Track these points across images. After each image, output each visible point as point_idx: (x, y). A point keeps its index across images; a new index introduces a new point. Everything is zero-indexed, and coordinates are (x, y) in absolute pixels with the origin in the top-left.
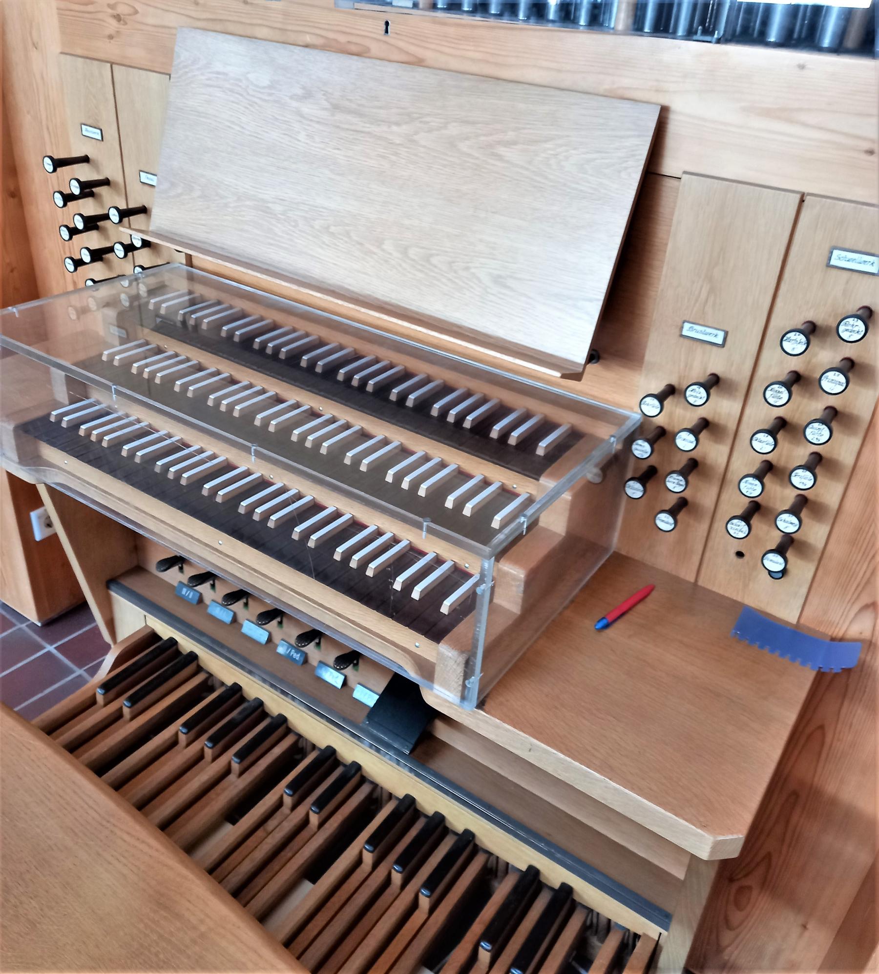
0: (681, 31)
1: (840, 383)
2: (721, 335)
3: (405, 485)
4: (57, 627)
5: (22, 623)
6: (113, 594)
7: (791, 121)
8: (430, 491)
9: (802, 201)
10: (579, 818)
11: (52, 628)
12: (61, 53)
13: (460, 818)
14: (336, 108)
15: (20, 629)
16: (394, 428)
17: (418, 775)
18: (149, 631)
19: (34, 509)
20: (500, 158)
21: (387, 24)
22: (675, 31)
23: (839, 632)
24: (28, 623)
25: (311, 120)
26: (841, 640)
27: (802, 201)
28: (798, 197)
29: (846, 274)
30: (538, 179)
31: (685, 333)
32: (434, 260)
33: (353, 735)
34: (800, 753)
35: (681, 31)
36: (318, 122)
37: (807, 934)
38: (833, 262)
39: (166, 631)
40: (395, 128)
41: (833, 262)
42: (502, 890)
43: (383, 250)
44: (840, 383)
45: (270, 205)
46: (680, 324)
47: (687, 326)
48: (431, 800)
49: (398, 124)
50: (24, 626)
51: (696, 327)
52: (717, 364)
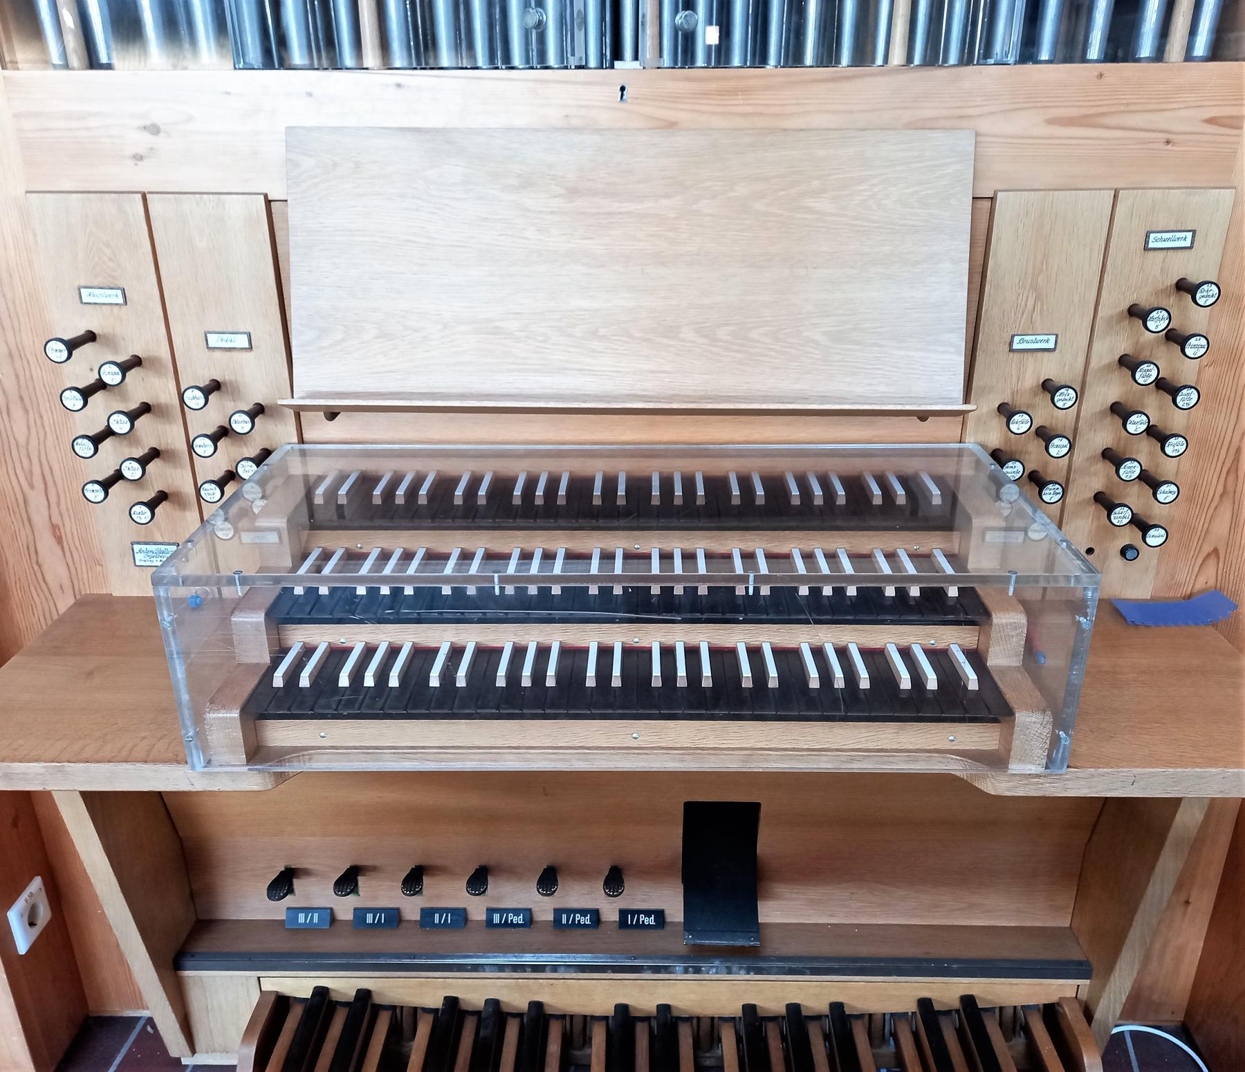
0: (953, 57)
1: (1202, 347)
2: (1053, 338)
7: (1094, 126)
8: (404, 678)
9: (1116, 197)
10: (935, 923)
12: (27, 192)
13: (814, 993)
14: (573, 192)
17: (759, 971)
18: (273, 998)
20: (810, 210)
21: (623, 89)
22: (945, 60)
23: (1187, 590)
25: (541, 212)
26: (1190, 596)
27: (1116, 197)
28: (1112, 193)
29: (1163, 253)
30: (858, 223)
31: (1015, 346)
32: (753, 335)
33: (656, 970)
34: (501, 968)
35: (953, 57)
36: (552, 213)
37: (1190, 908)
38: (1151, 245)
39: (299, 985)
40: (665, 202)
41: (1151, 245)
43: (683, 340)
44: (1202, 347)
45: (498, 324)
46: (1008, 340)
47: (1017, 339)
48: (773, 993)
49: (667, 196)
51: (1026, 338)
52: (1050, 369)
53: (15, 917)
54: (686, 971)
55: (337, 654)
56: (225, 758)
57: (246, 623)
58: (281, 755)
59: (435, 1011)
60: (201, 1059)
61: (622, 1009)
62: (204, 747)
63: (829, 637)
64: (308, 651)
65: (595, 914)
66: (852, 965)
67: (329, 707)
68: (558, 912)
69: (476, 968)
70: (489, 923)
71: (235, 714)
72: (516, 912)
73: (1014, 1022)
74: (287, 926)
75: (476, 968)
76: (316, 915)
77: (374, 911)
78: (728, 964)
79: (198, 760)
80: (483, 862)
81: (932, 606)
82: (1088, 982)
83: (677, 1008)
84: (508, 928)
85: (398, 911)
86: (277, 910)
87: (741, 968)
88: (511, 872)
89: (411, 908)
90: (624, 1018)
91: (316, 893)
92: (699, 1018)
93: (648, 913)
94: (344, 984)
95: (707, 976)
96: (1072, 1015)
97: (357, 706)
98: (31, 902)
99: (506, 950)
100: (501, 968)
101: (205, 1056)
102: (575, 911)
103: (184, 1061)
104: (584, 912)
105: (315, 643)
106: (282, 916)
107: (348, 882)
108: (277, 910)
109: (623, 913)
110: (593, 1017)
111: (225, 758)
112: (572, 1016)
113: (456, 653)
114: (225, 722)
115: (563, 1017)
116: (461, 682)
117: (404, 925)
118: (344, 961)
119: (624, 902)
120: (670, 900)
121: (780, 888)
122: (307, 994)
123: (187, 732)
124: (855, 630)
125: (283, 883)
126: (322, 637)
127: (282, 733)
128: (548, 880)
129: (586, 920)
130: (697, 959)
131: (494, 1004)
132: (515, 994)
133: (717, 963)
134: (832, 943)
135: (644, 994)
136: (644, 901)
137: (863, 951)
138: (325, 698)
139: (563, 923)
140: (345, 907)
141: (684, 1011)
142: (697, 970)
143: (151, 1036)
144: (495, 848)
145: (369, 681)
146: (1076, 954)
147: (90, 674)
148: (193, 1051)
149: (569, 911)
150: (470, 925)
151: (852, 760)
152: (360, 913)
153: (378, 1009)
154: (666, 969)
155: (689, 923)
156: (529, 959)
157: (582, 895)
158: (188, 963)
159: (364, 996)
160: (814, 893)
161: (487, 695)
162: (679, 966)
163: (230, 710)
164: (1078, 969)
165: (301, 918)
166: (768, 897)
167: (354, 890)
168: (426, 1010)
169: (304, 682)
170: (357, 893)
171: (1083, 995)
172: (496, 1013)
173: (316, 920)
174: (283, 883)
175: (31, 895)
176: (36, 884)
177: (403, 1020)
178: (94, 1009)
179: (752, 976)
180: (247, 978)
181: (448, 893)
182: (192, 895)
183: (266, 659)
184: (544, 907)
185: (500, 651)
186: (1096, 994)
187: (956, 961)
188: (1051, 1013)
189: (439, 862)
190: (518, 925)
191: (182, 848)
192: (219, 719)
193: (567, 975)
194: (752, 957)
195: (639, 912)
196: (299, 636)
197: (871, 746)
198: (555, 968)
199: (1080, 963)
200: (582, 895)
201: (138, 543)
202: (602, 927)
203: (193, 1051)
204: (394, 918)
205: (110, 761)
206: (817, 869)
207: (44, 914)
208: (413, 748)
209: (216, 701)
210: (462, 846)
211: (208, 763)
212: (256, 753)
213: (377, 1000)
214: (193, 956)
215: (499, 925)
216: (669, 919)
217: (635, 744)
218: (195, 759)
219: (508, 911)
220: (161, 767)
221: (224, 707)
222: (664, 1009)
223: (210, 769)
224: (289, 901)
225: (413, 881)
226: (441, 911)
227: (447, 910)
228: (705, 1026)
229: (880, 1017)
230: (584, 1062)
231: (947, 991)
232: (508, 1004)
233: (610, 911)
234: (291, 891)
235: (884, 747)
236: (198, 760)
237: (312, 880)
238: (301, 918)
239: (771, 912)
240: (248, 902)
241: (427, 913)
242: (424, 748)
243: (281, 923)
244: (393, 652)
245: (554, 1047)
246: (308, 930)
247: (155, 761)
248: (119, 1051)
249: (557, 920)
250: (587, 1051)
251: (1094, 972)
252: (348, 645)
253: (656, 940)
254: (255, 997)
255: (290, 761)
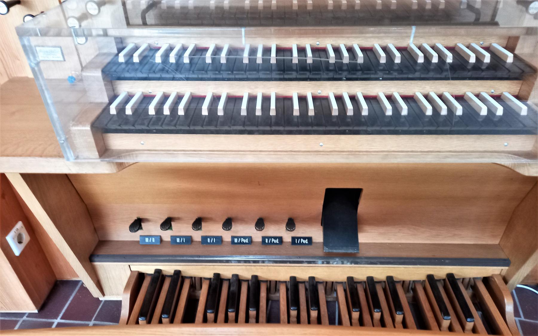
3: (166, 111)
4: (50, 306)
5: (22, 317)
6: (97, 264)
8: (187, 110)
11: (46, 309)
13: (380, 272)
15: (24, 321)
16: (302, 35)
17: (356, 263)
18: (136, 274)
19: (7, 232)
24: (26, 315)
39: (148, 268)
42: (203, 294)
48: (361, 272)
50: (25, 318)
53: (10, 239)
54: (323, 263)
55: (147, 98)
56: (86, 154)
57: (91, 76)
58: (120, 154)
59: (210, 279)
60: (108, 298)
61: (293, 279)
62: (73, 147)
63: (433, 88)
64: (129, 97)
65: (280, 239)
66: (395, 261)
67: (143, 124)
68: (264, 238)
69: (228, 261)
70: (233, 242)
71: (88, 128)
72: (245, 238)
73: (472, 285)
74: (140, 243)
75: (228, 261)
76: (153, 239)
77: (180, 237)
78: (343, 260)
79: (70, 154)
80: (229, 216)
81: (495, 70)
82: (507, 268)
83: (318, 278)
84: (241, 244)
85: (191, 237)
86: (136, 236)
87: (348, 262)
88: (243, 221)
89: (197, 236)
90: (294, 283)
91: (152, 229)
92: (326, 282)
93: (305, 238)
94: (168, 268)
95: (332, 265)
96: (499, 282)
97: (160, 124)
98: (18, 233)
99: (241, 254)
100: (239, 261)
101: (109, 297)
102: (271, 237)
103: (101, 299)
104: (275, 238)
105: (134, 92)
106: (138, 239)
107: (167, 224)
108: (136, 236)
109: (293, 238)
110: (280, 282)
111: (86, 154)
112: (270, 281)
113: (216, 99)
114: (83, 133)
115: (267, 281)
116: (220, 113)
117: (193, 243)
118: (168, 258)
119: (295, 234)
120: (317, 234)
121: (367, 228)
122: (152, 272)
123: (61, 138)
124: (448, 84)
125: (137, 225)
126: (137, 89)
127: (118, 141)
128: (260, 224)
129: (277, 241)
130: (328, 258)
131: (236, 276)
132: (246, 272)
133: (337, 259)
134: (387, 253)
135: (303, 272)
136: (303, 233)
137: (404, 254)
138: (143, 121)
139: (266, 242)
140: (167, 235)
141: (320, 279)
142: (328, 263)
143: (84, 290)
144: (234, 209)
145: (166, 111)
146: (502, 256)
147: (13, 113)
148: (104, 295)
149: (269, 238)
150: (224, 243)
151: (447, 157)
152: (174, 238)
153: (184, 278)
154: (314, 262)
155: (326, 242)
156: (251, 258)
157: (273, 230)
158: (96, 259)
159: (178, 273)
160: (382, 230)
161: (234, 121)
162: (320, 261)
163: (84, 125)
164: (505, 262)
165: (147, 240)
166: (363, 231)
167: (170, 228)
168: (205, 279)
169: (129, 111)
170: (172, 229)
171: (504, 273)
172: (237, 280)
173: (153, 241)
174: (137, 225)
175: (17, 229)
176: (20, 225)
177: (195, 283)
178: (59, 277)
179: (353, 265)
180: (124, 265)
181: (214, 229)
182: (95, 230)
183: (106, 100)
184: (257, 236)
185: (241, 98)
186: (512, 274)
187: (448, 259)
188: (486, 281)
189: (209, 216)
190: (246, 243)
191: (87, 208)
192: (79, 130)
193: (269, 265)
194: (354, 258)
195: (300, 238)
196: (125, 88)
197: (458, 149)
198: (263, 262)
199: (505, 260)
200: (273, 230)
201: (39, 46)
202: (284, 244)
203: (104, 295)
204: (189, 240)
205: (21, 156)
206: (384, 220)
207: (26, 238)
208: (195, 151)
209: (78, 120)
210: (218, 208)
211: (77, 158)
212: (104, 151)
213: (184, 274)
214: (98, 256)
215: (238, 243)
216: (314, 240)
217: (321, 149)
218: (69, 155)
219: (241, 237)
220: (49, 159)
221: (81, 123)
222: (312, 279)
223: (79, 160)
224: (140, 232)
225: (198, 224)
226: (210, 237)
227: (213, 237)
228: (329, 286)
229: (408, 282)
230: (276, 299)
231: (440, 271)
232: (242, 276)
233: (287, 237)
234: (140, 228)
235: (466, 150)
236: (70, 154)
237: (150, 223)
238: (147, 240)
239: (364, 238)
240: (121, 233)
241: (204, 238)
242: (201, 151)
243: (138, 242)
244: (179, 98)
245: (263, 294)
246: (151, 245)
247: (47, 156)
248: (71, 295)
249: (263, 241)
250: (277, 295)
251: (511, 264)
252: (153, 94)
253: (310, 250)
254: (129, 273)
255: (125, 156)
